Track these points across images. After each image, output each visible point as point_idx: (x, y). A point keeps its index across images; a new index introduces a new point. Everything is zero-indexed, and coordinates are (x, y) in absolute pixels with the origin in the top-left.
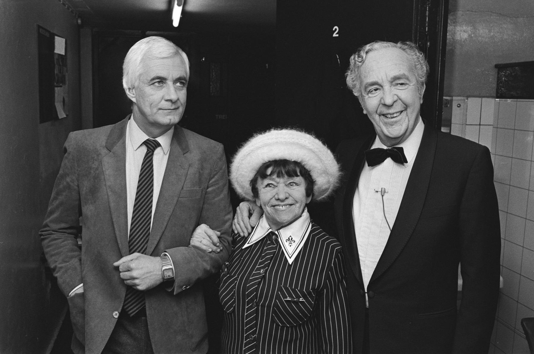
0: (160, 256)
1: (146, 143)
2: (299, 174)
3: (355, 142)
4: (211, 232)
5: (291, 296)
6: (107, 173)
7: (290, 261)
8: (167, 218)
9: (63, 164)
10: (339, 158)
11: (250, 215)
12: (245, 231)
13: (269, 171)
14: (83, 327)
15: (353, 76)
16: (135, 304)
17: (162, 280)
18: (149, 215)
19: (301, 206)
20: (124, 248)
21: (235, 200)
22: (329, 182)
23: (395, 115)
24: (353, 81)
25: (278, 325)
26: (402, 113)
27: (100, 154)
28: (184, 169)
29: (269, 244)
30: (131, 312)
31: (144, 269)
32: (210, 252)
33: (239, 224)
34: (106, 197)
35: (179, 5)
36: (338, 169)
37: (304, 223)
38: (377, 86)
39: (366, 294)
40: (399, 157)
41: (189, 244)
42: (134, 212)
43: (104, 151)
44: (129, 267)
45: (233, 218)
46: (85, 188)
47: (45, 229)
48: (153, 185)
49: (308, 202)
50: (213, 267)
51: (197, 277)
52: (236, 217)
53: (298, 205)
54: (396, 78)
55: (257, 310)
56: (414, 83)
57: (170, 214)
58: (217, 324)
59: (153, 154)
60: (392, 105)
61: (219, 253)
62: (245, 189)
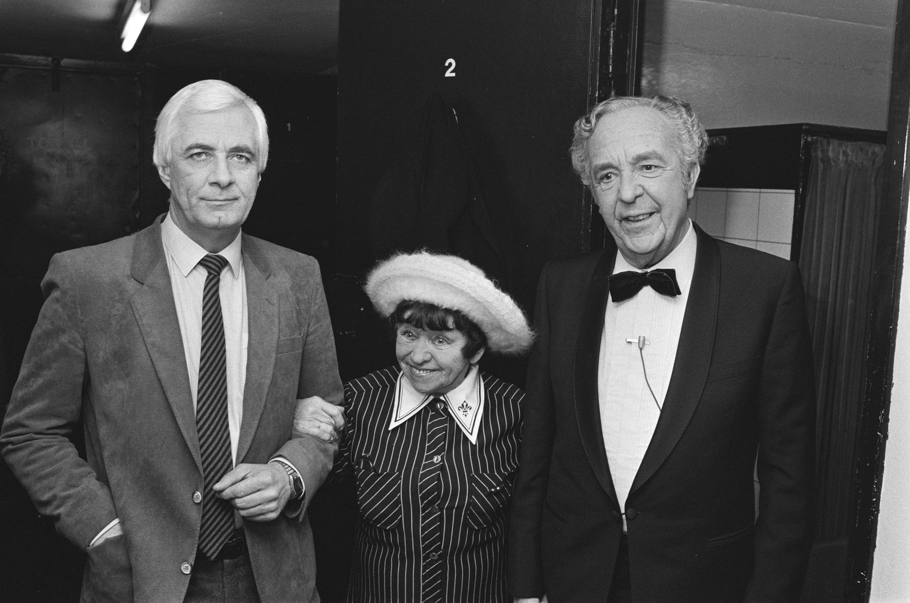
1: (202, 263)
23: (641, 218)
24: (582, 161)
26: (653, 216)
30: (211, 551)
35: (143, 10)
38: (607, 172)
40: (666, 284)
42: (228, 425)
43: (131, 285)
46: (101, 353)
54: (640, 158)
56: (674, 165)
60: (633, 202)
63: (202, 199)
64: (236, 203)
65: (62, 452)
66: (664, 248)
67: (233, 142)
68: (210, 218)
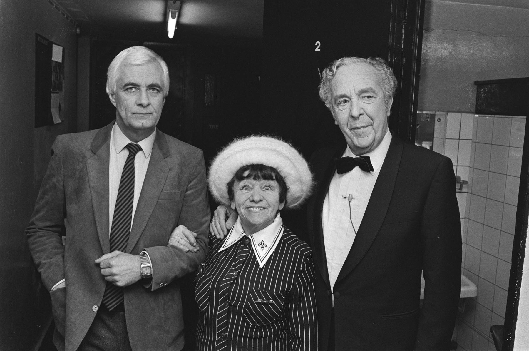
0: (139, 254)
1: (128, 147)
2: (274, 178)
3: (328, 153)
4: (188, 232)
5: (261, 298)
6: (91, 174)
7: (261, 265)
8: (147, 219)
9: (49, 166)
10: (313, 168)
11: (227, 218)
12: (221, 233)
13: (246, 174)
14: (64, 321)
15: (325, 88)
16: (114, 299)
17: (140, 278)
18: (129, 215)
19: (273, 210)
20: (106, 246)
21: (213, 204)
22: (302, 190)
24: (326, 93)
25: (248, 324)
27: (85, 157)
28: (164, 173)
29: (243, 248)
31: (124, 267)
32: (187, 252)
33: (216, 226)
34: (90, 197)
36: (311, 179)
37: (276, 227)
38: (346, 99)
39: (333, 295)
40: (367, 167)
41: (168, 244)
42: (115, 212)
43: (89, 154)
44: (109, 264)
45: (211, 221)
47: (31, 227)
48: (134, 187)
49: (281, 208)
50: (191, 266)
51: (174, 275)
52: (213, 219)
53: (270, 209)
54: (363, 91)
55: (230, 309)
57: (149, 214)
58: (193, 320)
59: (134, 157)
61: (195, 252)
62: (221, 193)
63: (134, 114)
64: (151, 116)
65: (50, 240)
66: (375, 145)
67: (150, 82)
68: (138, 123)
